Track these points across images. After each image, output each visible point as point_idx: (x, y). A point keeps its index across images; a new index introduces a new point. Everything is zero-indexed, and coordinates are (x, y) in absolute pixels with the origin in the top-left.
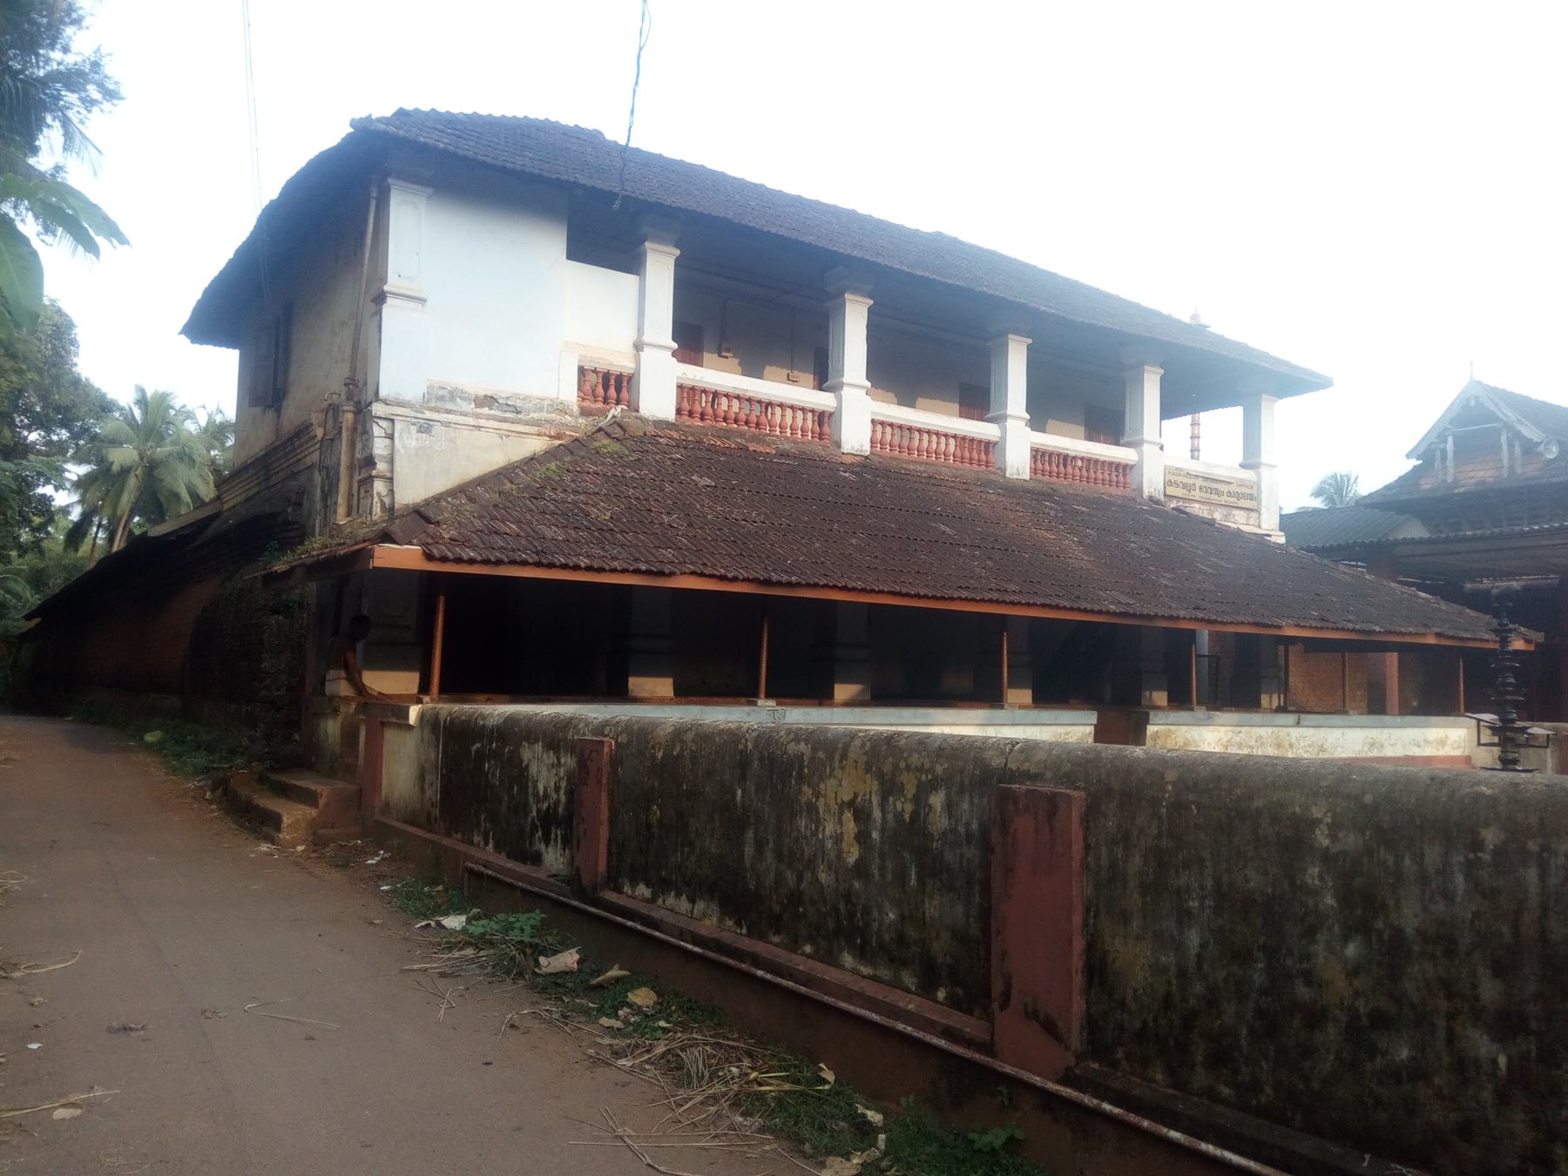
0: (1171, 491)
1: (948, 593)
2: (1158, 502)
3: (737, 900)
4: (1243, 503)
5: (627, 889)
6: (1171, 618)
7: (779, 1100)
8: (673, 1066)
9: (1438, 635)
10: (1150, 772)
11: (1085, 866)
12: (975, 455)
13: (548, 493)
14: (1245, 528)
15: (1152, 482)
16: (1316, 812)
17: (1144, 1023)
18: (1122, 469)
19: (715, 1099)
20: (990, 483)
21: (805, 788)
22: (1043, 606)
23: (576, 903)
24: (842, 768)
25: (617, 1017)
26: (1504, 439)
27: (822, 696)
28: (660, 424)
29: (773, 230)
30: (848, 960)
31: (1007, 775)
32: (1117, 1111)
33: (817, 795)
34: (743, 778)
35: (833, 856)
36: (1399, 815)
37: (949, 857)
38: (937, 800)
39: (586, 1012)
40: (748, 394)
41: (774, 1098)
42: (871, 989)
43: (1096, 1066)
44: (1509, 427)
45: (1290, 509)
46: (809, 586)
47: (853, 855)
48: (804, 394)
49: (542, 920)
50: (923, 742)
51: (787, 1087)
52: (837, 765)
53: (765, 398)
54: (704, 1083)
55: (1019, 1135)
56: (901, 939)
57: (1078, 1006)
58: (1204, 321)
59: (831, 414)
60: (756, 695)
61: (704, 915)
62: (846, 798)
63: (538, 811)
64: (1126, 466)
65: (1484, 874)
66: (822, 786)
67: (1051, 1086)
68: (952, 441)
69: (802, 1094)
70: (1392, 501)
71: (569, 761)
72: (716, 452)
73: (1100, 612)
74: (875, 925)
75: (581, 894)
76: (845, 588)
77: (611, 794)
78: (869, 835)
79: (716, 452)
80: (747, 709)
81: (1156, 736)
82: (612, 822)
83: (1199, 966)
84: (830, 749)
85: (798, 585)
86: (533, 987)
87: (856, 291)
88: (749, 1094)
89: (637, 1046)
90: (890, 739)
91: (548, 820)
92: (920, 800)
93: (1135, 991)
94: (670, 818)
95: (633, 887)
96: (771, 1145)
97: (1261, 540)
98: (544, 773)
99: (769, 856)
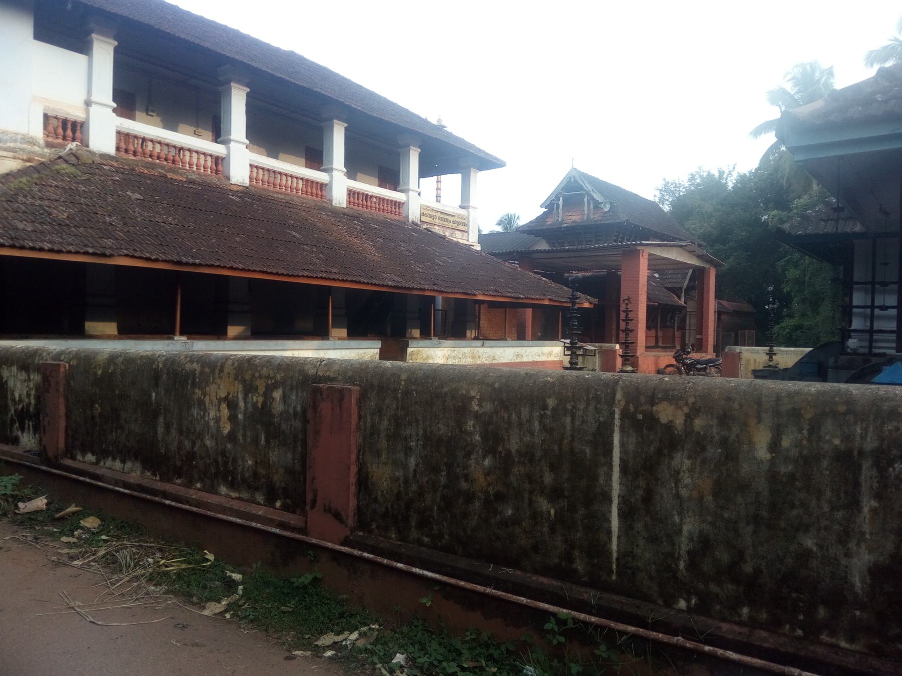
0: (424, 219)
1: (296, 273)
2: (416, 225)
3: (151, 457)
4: (460, 227)
5: (79, 457)
6: (421, 289)
7: (179, 575)
8: (111, 563)
9: (550, 300)
10: (394, 375)
11: (359, 427)
12: (314, 191)
13: (20, 198)
14: (461, 241)
15: (414, 213)
16: (473, 393)
17: (387, 508)
18: (398, 205)
19: (137, 578)
20: (323, 209)
21: (197, 391)
22: (352, 281)
23: (44, 468)
24: (220, 378)
25: (73, 536)
26: (586, 200)
27: (219, 333)
28: (103, 156)
29: (183, 36)
30: (223, 490)
31: (317, 379)
32: (371, 556)
33: (205, 394)
34: (157, 385)
35: (214, 430)
36: (513, 394)
37: (284, 427)
38: (277, 394)
39: (52, 534)
40: (167, 141)
41: (175, 574)
42: (236, 505)
43: (361, 533)
44: (589, 194)
45: (485, 232)
46: (207, 266)
47: (227, 429)
48: (205, 144)
49: (21, 480)
50: (269, 361)
51: (184, 566)
52: (217, 376)
53: (179, 145)
54: (130, 569)
55: (319, 576)
56: (255, 475)
57: (353, 503)
58: (444, 123)
59: (223, 159)
60: (174, 333)
61: (132, 470)
62: (223, 396)
63: (16, 410)
64: (400, 203)
65: (547, 421)
66: (207, 389)
67: (338, 547)
68: (300, 181)
69: (193, 569)
70: (535, 230)
71: (36, 378)
72: (145, 177)
73: (383, 286)
74: (240, 469)
75: (49, 462)
76: (231, 268)
77: (66, 398)
78: (237, 417)
79: (145, 177)
80: (167, 342)
81: (412, 353)
82: (68, 417)
83: (415, 476)
84: (213, 368)
85: (200, 265)
86: (13, 522)
87: (239, 82)
88: (159, 574)
89: (86, 552)
90: (250, 360)
91: (23, 416)
92: (267, 395)
93: (383, 492)
94: (105, 409)
95: (83, 456)
96: (172, 600)
97: (468, 248)
98: (19, 385)
99: (174, 433)
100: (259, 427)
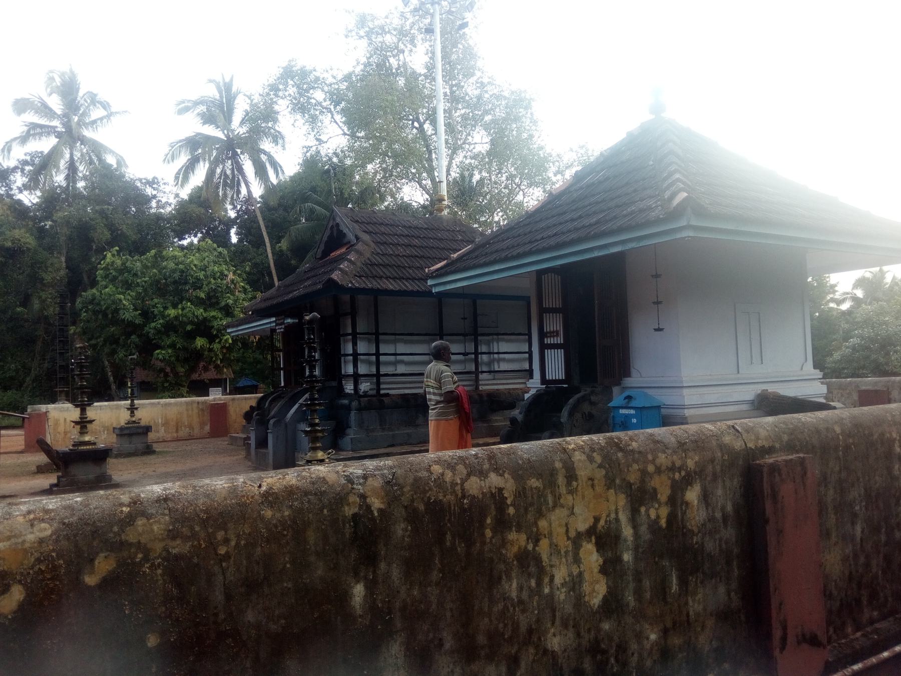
24: (570, 492)
35: (569, 609)
47: (597, 591)
52: (563, 490)
62: (583, 527)
78: (619, 559)
92: (675, 500)
100: (666, 563)
